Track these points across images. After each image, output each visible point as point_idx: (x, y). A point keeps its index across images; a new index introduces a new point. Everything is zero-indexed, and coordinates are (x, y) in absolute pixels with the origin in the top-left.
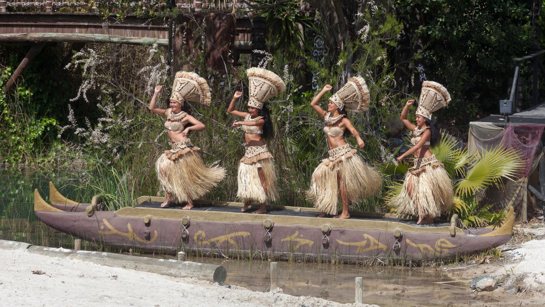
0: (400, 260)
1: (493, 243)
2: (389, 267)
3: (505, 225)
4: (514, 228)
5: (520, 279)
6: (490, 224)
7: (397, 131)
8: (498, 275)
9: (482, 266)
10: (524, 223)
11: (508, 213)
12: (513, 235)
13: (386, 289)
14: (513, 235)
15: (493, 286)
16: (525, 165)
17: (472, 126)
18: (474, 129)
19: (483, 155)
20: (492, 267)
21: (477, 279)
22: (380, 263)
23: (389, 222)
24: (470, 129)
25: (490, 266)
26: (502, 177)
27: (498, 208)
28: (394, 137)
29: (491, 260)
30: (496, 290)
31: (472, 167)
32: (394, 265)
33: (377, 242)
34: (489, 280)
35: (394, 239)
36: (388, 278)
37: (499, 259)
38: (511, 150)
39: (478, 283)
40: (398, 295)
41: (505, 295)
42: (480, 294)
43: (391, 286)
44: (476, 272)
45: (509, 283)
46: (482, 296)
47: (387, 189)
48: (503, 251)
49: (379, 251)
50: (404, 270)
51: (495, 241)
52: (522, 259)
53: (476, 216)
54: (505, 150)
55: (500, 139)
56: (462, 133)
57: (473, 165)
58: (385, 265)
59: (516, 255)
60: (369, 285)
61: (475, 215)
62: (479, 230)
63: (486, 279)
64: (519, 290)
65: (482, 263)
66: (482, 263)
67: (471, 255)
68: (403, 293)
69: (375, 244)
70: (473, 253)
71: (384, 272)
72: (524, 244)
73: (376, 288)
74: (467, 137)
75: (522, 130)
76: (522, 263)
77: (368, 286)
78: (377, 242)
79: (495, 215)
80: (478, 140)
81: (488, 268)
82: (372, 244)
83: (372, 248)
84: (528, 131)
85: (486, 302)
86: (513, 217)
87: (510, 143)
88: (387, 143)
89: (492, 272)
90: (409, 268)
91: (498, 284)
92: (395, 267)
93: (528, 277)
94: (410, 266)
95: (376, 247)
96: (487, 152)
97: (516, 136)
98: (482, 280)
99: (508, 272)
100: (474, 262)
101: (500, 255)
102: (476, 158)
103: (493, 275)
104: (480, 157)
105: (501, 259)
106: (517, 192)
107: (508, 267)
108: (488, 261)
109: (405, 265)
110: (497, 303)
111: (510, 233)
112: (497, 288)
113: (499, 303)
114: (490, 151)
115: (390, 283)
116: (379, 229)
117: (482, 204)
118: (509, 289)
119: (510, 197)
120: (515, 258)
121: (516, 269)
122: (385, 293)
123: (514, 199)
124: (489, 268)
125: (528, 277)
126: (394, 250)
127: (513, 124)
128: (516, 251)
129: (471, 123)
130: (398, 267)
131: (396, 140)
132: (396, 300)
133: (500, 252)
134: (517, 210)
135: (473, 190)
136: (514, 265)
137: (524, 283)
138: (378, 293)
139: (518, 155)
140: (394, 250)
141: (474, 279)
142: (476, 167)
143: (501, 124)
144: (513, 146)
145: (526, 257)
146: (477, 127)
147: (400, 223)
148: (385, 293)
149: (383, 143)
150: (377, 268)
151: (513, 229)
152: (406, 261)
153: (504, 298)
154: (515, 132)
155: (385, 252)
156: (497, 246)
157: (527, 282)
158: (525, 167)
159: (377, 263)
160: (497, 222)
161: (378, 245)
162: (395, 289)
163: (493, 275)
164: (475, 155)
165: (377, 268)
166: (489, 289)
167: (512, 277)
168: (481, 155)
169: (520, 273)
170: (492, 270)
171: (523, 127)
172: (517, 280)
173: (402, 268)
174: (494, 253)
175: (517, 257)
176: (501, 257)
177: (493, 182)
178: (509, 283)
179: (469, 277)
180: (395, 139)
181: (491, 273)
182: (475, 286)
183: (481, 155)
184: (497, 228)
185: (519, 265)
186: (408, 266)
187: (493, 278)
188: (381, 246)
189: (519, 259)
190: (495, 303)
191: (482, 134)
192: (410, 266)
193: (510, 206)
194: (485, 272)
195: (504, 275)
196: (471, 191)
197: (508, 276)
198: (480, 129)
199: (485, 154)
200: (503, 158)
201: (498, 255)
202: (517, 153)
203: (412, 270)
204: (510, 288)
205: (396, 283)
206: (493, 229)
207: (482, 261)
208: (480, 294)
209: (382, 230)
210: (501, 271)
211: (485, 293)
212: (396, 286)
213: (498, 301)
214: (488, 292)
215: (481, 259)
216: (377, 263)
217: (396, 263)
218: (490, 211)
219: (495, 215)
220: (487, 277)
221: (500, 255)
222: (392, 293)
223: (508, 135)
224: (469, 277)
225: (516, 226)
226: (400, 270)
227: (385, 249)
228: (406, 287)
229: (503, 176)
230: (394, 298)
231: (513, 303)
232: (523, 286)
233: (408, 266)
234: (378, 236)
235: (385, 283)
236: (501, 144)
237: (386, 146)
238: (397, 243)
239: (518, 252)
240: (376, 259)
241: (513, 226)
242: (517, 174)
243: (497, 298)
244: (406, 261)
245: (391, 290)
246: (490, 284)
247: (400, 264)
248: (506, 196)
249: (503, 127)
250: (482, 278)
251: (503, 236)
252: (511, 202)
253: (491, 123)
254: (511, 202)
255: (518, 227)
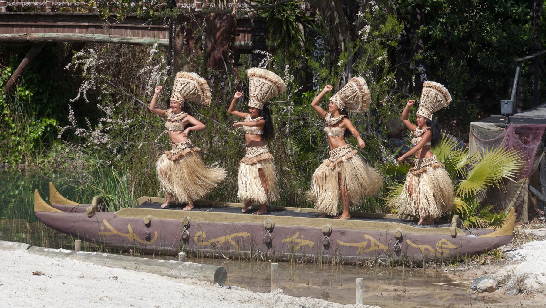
0: (401, 261)
1: (494, 244)
2: (390, 268)
3: (506, 225)
4: (515, 229)
5: (521, 280)
6: (491, 225)
7: (398, 132)
8: (499, 276)
9: (483, 267)
10: (525, 224)
11: (509, 214)
12: (514, 235)
13: (387, 290)
14: (514, 235)
15: (494, 287)
16: (526, 165)
17: (473, 126)
18: (475, 129)
19: (484, 156)
20: (493, 268)
21: (477, 280)
22: (381, 264)
23: (389, 223)
24: (471, 129)
25: (491, 267)
26: (503, 177)
27: (498, 209)
28: (394, 138)
29: (492, 261)
30: (497, 291)
31: (473, 168)
32: (395, 266)
33: (377, 243)
34: (490, 281)
35: (395, 240)
36: (389, 279)
37: (500, 260)
38: (512, 150)
39: (479, 284)
40: (398, 296)
41: (506, 296)
42: (481, 295)
43: (392, 287)
44: (477, 273)
45: (510, 284)
46: (483, 297)
47: (388, 190)
48: (503, 252)
49: (380, 252)
50: (405, 271)
51: (496, 241)
52: (523, 259)
53: (476, 217)
54: (506, 151)
55: (500, 139)
56: (463, 133)
57: (474, 165)
58: (386, 266)
59: (517, 256)
60: (370, 286)
61: (476, 215)
62: (480, 230)
63: (486, 280)
64: (520, 291)
65: (483, 264)
66: (483, 264)
67: (472, 256)
68: (404, 294)
69: (376, 245)
70: (474, 254)
71: (385, 273)
72: (525, 245)
73: (377, 289)
74: (468, 138)
75: (523, 131)
76: (523, 264)
77: (368, 287)
78: (377, 243)
79: (496, 216)
80: (479, 140)
81: (489, 269)
82: (373, 244)
83: (372, 248)
84: (529, 132)
85: (487, 303)
86: (513, 218)
87: (511, 143)
88: (387, 144)
89: (493, 273)
90: (410, 269)
91: (499, 285)
92: (395, 268)
93: (529, 278)
94: (411, 267)
95: (377, 248)
96: (488, 152)
97: (517, 136)
98: (483, 281)
99: (509, 273)
100: (475, 263)
101: (501, 256)
102: (477, 159)
103: (494, 275)
104: (481, 158)
105: (502, 260)
106: (518, 192)
107: (509, 268)
108: (489, 262)
109: (406, 266)
110: (498, 304)
111: (511, 234)
112: (498, 289)
113: (500, 304)
114: (491, 151)
115: (390, 284)
116: (379, 229)
117: (483, 205)
118: (510, 290)
119: (511, 197)
120: (516, 259)
121: (517, 269)
122: (385, 294)
123: (515, 199)
124: (490, 268)
125: (529, 278)
126: (395, 251)
127: (514, 124)
128: (517, 251)
129: (472, 123)
130: (398, 268)
131: (397, 141)
132: (396, 301)
133: (501, 253)
134: (518, 210)
135: (474, 190)
136: (515, 266)
137: (525, 284)
138: (379, 294)
139: (519, 156)
140: (395, 251)
141: (474, 280)
142: (477, 167)
143: (501, 124)
144: (514, 147)
145: (526, 258)
146: (477, 127)
147: (401, 224)
148: (385, 294)
149: (384, 143)
150: (377, 269)
151: (514, 230)
152: (407, 262)
153: (504, 299)
154: (516, 133)
155: (386, 253)
156: (498, 247)
157: (528, 283)
158: (526, 168)
159: (377, 264)
160: (498, 223)
161: (379, 246)
162: (396, 290)
163: (494, 275)
164: (476, 155)
165: (377, 269)
166: (490, 289)
167: (513, 277)
168: (482, 156)
169: (521, 274)
170: (493, 271)
171: (524, 128)
172: (518, 281)
173: (403, 269)
174: (495, 254)
175: (518, 258)
176: (502, 258)
177: (494, 183)
178: (510, 284)
179: (470, 278)
180: (395, 139)
181: (491, 273)
182: (475, 287)
183: (482, 156)
184: (498, 229)
185: (520, 266)
186: (409, 267)
187: (494, 279)
188: (382, 246)
189: (520, 260)
190: (495, 304)
191: (483, 134)
192: (411, 267)
193: (511, 207)
194: (486, 273)
195: (504, 276)
196: (472, 191)
197: (509, 276)
198: (481, 129)
199: (485, 154)
200: (504, 158)
201: (499, 255)
202: (518, 153)
203: (413, 271)
204: (511, 289)
205: (397, 284)
206: (494, 230)
207: (483, 262)
208: (481, 295)
209: (383, 230)
210: (502, 272)
211: (486, 294)
212: (396, 287)
213: (499, 302)
214: (489, 293)
215: (482, 260)
216: (377, 264)
217: (396, 263)
218: (491, 211)
219: (496, 216)
220: (487, 278)
221: (501, 256)
222: (393, 294)
223: (509, 136)
224: (470, 278)
225: (517, 226)
226: (401, 271)
227: (385, 250)
228: (406, 288)
229: (504, 176)
230: (394, 299)
231: (514, 304)
232: (524, 287)
233: (409, 267)
234: (379, 237)
235: (386, 284)
236: (502, 145)
237: (387, 146)
238: (398, 244)
239: (519, 253)
240: (376, 260)
241: (514, 227)
242: (518, 175)
243: (498, 299)
244: (407, 262)
245: (392, 291)
246: (491, 285)
247: (401, 265)
248: (507, 196)
249: (504, 127)
250: (483, 278)
251: (504, 237)
252: (512, 203)
253: (491, 124)
254: (512, 203)
255: (519, 228)
